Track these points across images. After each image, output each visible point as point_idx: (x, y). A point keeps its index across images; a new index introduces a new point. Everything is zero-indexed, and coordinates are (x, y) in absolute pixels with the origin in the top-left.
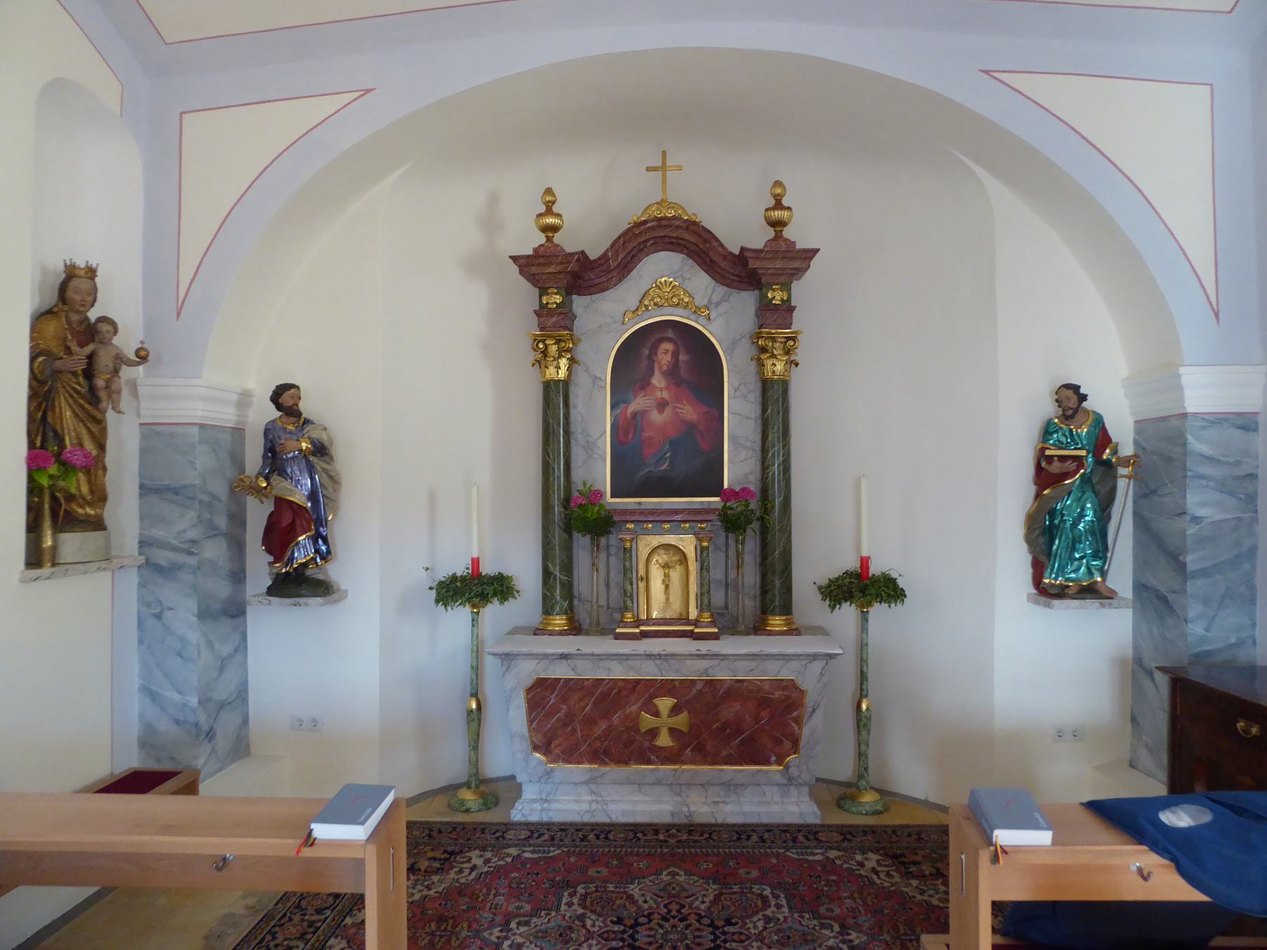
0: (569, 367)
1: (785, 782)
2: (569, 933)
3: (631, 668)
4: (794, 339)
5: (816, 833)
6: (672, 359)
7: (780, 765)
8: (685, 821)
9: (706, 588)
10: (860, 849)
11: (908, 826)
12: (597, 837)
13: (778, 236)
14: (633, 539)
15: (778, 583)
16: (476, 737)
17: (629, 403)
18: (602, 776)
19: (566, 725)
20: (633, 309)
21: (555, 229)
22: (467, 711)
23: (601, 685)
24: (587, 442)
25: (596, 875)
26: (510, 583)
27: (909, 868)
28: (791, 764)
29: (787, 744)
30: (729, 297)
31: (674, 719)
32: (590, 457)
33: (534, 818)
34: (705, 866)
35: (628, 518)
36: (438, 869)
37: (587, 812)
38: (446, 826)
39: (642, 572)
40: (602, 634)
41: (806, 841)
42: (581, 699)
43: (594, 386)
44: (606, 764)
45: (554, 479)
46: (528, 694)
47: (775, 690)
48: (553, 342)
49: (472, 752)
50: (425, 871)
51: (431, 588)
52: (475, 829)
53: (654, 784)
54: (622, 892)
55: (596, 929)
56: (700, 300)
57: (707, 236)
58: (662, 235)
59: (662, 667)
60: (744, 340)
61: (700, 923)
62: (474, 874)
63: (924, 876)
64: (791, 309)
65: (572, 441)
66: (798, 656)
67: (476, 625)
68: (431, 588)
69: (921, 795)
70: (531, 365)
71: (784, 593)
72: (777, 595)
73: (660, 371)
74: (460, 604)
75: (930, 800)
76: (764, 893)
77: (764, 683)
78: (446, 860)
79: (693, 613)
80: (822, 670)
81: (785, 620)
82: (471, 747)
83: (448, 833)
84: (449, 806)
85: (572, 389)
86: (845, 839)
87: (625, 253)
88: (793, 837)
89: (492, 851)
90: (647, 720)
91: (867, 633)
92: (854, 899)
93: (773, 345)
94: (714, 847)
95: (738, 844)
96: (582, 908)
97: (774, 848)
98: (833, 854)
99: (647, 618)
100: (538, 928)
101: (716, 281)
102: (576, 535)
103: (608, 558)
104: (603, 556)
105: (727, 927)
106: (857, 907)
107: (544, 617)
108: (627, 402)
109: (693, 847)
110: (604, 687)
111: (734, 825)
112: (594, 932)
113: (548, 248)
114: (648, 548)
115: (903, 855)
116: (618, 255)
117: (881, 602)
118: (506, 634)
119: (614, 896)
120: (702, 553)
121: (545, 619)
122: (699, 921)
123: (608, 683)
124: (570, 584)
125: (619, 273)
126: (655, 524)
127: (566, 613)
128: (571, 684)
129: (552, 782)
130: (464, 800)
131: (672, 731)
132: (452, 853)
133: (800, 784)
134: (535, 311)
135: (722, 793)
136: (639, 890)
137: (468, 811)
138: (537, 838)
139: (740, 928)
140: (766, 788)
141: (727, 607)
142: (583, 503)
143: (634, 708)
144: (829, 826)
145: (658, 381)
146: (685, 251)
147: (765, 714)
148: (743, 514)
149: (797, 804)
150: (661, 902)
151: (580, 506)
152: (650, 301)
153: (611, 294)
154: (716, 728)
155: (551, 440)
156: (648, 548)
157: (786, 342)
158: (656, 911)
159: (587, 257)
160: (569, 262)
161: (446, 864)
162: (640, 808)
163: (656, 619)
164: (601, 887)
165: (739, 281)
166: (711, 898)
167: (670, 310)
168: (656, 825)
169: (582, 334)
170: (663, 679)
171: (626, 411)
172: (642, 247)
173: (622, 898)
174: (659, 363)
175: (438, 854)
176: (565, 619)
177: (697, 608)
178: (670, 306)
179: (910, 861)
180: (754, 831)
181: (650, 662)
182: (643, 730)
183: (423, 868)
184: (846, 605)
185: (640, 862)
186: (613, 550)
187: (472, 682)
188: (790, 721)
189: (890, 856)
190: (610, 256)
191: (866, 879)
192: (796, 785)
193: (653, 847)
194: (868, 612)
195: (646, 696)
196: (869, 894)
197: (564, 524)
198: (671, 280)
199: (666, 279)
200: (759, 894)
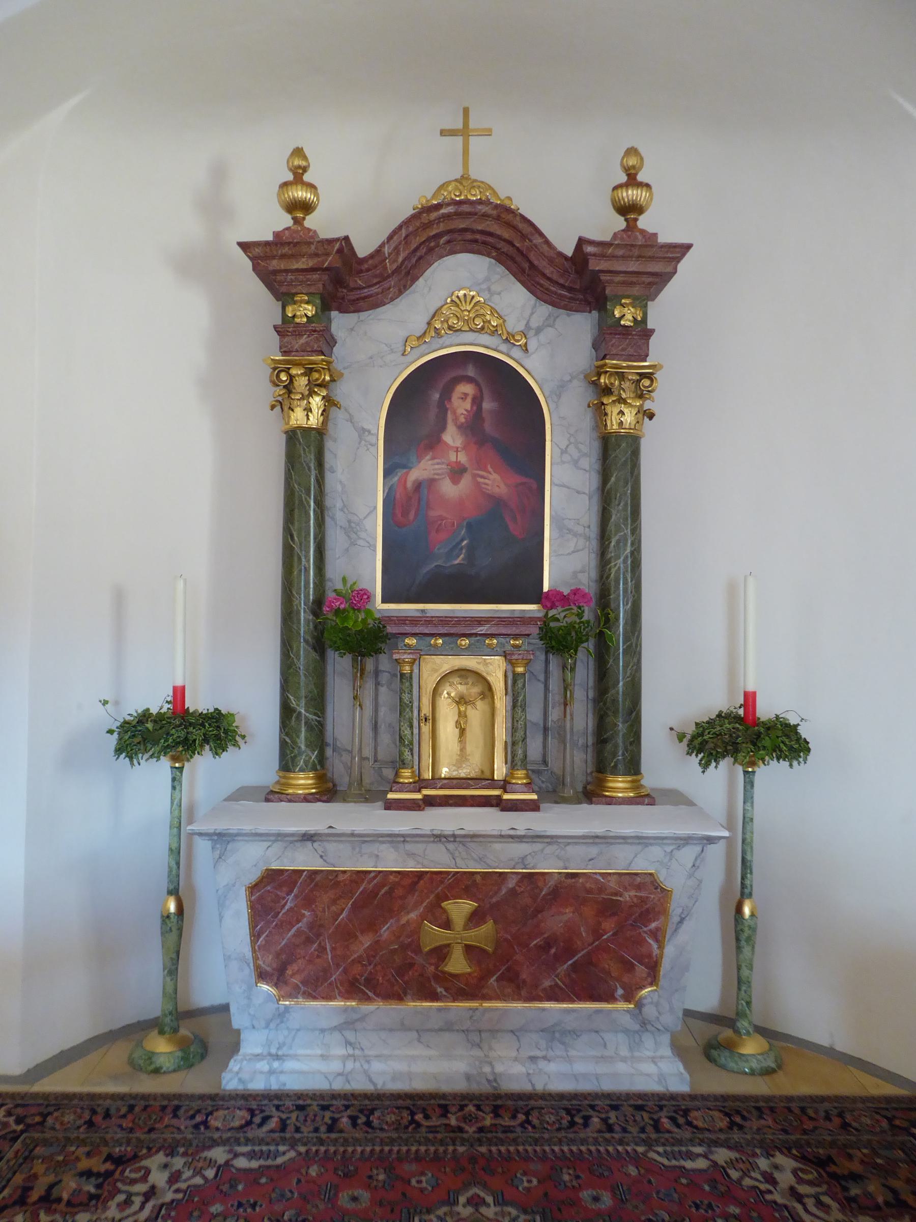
0: (324, 411)
1: (637, 1027)
3: (411, 855)
4: (649, 376)
5: (686, 1112)
7: (630, 1002)
8: (486, 1088)
9: (520, 734)
10: (762, 1144)
11: (822, 1099)
12: (353, 1120)
13: (631, 226)
14: (415, 660)
15: (621, 727)
16: (174, 956)
17: (411, 468)
18: (363, 1018)
19: (309, 941)
20: (419, 334)
21: (307, 207)
22: (162, 916)
23: (363, 880)
24: (349, 522)
25: (351, 1206)
26: (230, 725)
28: (645, 1001)
29: (641, 970)
30: (555, 320)
31: (473, 933)
32: (353, 544)
33: (258, 1085)
35: (408, 629)
36: (92, 1197)
37: (339, 1074)
38: (119, 1103)
39: (426, 710)
40: (367, 800)
41: (676, 1130)
42: (334, 902)
44: (368, 999)
45: (300, 571)
46: (252, 893)
47: (625, 889)
48: (302, 371)
49: (168, 979)
50: (69, 1203)
51: (110, 732)
52: (164, 1108)
53: (441, 1030)
56: (514, 324)
57: (526, 229)
58: (462, 226)
59: (457, 854)
60: (576, 383)
63: (878, 1208)
64: (647, 334)
65: (327, 519)
66: (660, 840)
67: (178, 788)
68: (110, 732)
69: (822, 1038)
70: (269, 408)
71: (631, 743)
72: (621, 744)
73: (456, 424)
74: (152, 756)
75: (839, 1047)
77: (609, 878)
78: (108, 1174)
79: (500, 771)
80: (696, 859)
81: (632, 781)
82: (166, 971)
84: (131, 1062)
85: (329, 445)
86: (732, 1125)
89: (185, 1154)
90: (433, 934)
91: (752, 803)
94: (536, 1141)
95: (571, 1136)
97: (628, 1144)
99: (433, 778)
101: (538, 298)
102: (331, 654)
103: (377, 690)
104: (370, 685)
107: (281, 774)
108: (407, 467)
111: (561, 1096)
113: (297, 232)
114: (436, 675)
116: (398, 254)
117: (778, 760)
118: (225, 800)
120: (514, 683)
121: (284, 777)
123: (375, 877)
124: (321, 725)
125: (400, 280)
126: (447, 638)
127: (314, 769)
128: (318, 878)
130: (153, 1053)
131: (469, 949)
134: (275, 327)
135: (543, 1044)
137: (157, 1071)
138: (260, 1125)
140: (608, 1036)
141: (545, 762)
142: (342, 606)
143: (413, 915)
144: (704, 1098)
145: (452, 437)
146: (494, 254)
147: (609, 925)
148: (574, 627)
149: (654, 1060)
151: (337, 612)
152: (442, 322)
153: (387, 312)
154: (535, 945)
155: (296, 516)
156: (436, 675)
157: (639, 381)
159: (352, 249)
160: (328, 255)
162: (418, 1067)
163: (445, 779)
165: (570, 298)
167: (471, 337)
168: (444, 1096)
169: (344, 368)
170: (458, 872)
171: (405, 482)
172: (432, 244)
174: (454, 413)
175: (98, 1165)
176: (312, 778)
177: (506, 763)
178: (471, 330)
180: (592, 1107)
181: (441, 847)
183: (65, 1196)
184: (725, 763)
186: (384, 678)
187: (170, 871)
188: (645, 935)
190: (387, 255)
194: (754, 772)
195: (432, 897)
197: (314, 637)
198: (472, 293)
199: (464, 292)
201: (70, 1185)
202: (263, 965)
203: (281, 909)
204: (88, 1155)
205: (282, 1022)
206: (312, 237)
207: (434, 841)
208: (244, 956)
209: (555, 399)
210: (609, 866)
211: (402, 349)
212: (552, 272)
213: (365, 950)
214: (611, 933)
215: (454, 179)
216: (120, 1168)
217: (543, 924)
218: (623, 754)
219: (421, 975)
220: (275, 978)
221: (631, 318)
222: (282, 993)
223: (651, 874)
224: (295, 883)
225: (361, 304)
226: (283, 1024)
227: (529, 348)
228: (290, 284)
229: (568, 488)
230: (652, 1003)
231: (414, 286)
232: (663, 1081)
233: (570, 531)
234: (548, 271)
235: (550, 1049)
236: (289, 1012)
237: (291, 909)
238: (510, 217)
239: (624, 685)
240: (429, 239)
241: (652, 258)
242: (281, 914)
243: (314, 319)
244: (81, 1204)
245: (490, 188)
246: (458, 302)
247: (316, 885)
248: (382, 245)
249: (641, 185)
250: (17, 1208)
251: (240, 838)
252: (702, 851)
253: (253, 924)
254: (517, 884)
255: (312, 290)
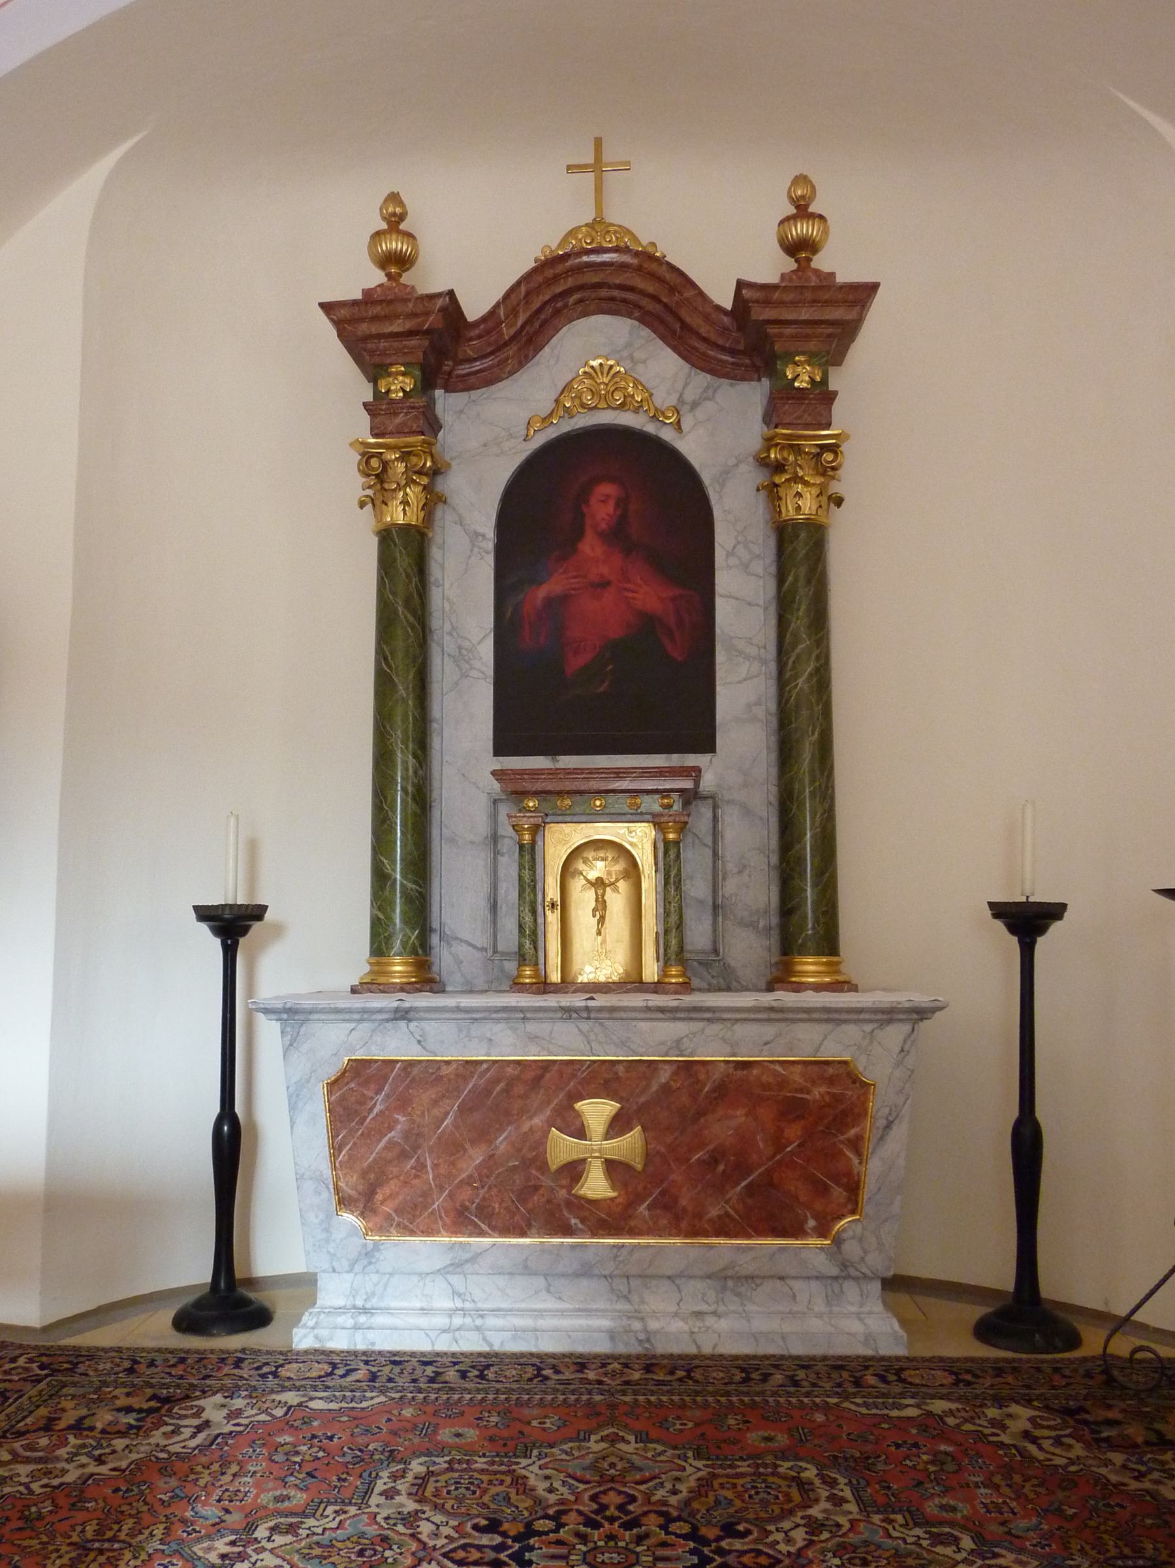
2: (379, 1549)
3: (533, 1038)
4: (834, 449)
6: (615, 510)
8: (635, 1349)
12: (463, 1375)
13: (804, 266)
19: (404, 1155)
20: (543, 416)
24: (460, 648)
27: (1099, 1432)
28: (845, 1236)
30: (715, 392)
34: (678, 1427)
36: (131, 1427)
37: (444, 1331)
39: (553, 892)
42: (435, 1103)
43: (472, 550)
46: (330, 1092)
47: (813, 1082)
50: (103, 1431)
52: (223, 1360)
54: (503, 1473)
55: (440, 1542)
56: (663, 398)
58: (597, 280)
59: (592, 1037)
60: (743, 468)
61: (668, 1533)
62: (201, 1437)
63: (1135, 1446)
64: (829, 398)
76: (803, 1475)
78: (151, 1411)
79: (651, 971)
80: (905, 1041)
81: (827, 964)
83: (170, 1366)
87: (528, 313)
88: (855, 1377)
92: (997, 1487)
93: (796, 460)
96: (416, 1501)
98: (938, 1406)
100: (315, 1538)
101: (693, 365)
105: (728, 1540)
106: (1005, 1502)
107: (374, 960)
109: (653, 1393)
110: (480, 1077)
111: (736, 1358)
112: (434, 1548)
115: (1081, 1409)
116: (516, 316)
119: (485, 1478)
121: (378, 964)
122: (664, 1527)
127: (414, 952)
129: (377, 1272)
131: (612, 1167)
132: (167, 1400)
133: (865, 1276)
134: (365, 405)
135: (712, 1295)
136: (540, 1468)
139: (756, 1541)
140: (797, 1285)
143: (537, 1121)
146: (637, 314)
147: (794, 1132)
150: (585, 1490)
157: (819, 455)
158: (576, 1507)
160: (427, 314)
161: (149, 1420)
164: (459, 1462)
166: (692, 1483)
168: (581, 1356)
170: (594, 1061)
172: (559, 305)
173: (502, 1482)
178: (610, 407)
179: (1100, 1419)
180: (776, 1367)
182: (554, 1165)
183: (99, 1426)
185: (546, 1417)
188: (841, 1146)
189: (1056, 1411)
191: (1014, 1451)
192: (856, 1279)
193: (573, 1392)
196: (1027, 1479)
198: (611, 362)
199: (600, 361)
200: (794, 1478)
201: (103, 1418)
202: (345, 1188)
203: (369, 1114)
204: (128, 1395)
205: (370, 1263)
206: (409, 293)
207: (562, 1018)
208: (321, 1175)
209: (718, 488)
210: (790, 1050)
211: (524, 432)
212: (708, 332)
213: (478, 1167)
214: (796, 1144)
215: (584, 223)
216: (167, 1407)
217: (706, 1132)
218: (813, 928)
219: (549, 1201)
220: (361, 1206)
221: (807, 378)
222: (370, 1225)
223: (845, 1063)
224: (385, 1079)
225: (472, 379)
226: (372, 1267)
227: (683, 426)
228: (384, 353)
229: (737, 599)
230: (853, 1238)
231: (538, 356)
232: (872, 1342)
233: (740, 652)
234: (704, 330)
235: (721, 1303)
236: (379, 1250)
237: (381, 1112)
238: (654, 267)
239: (811, 837)
240: (554, 298)
241: (828, 303)
242: (368, 1120)
243: (412, 393)
244: (119, 1432)
245: (628, 232)
246: (594, 374)
247: (413, 1080)
248: (497, 305)
249: (813, 216)
250: (42, 1433)
251: (315, 1016)
252: (913, 1030)
253: (334, 1133)
254: (671, 1079)
255: (408, 359)
